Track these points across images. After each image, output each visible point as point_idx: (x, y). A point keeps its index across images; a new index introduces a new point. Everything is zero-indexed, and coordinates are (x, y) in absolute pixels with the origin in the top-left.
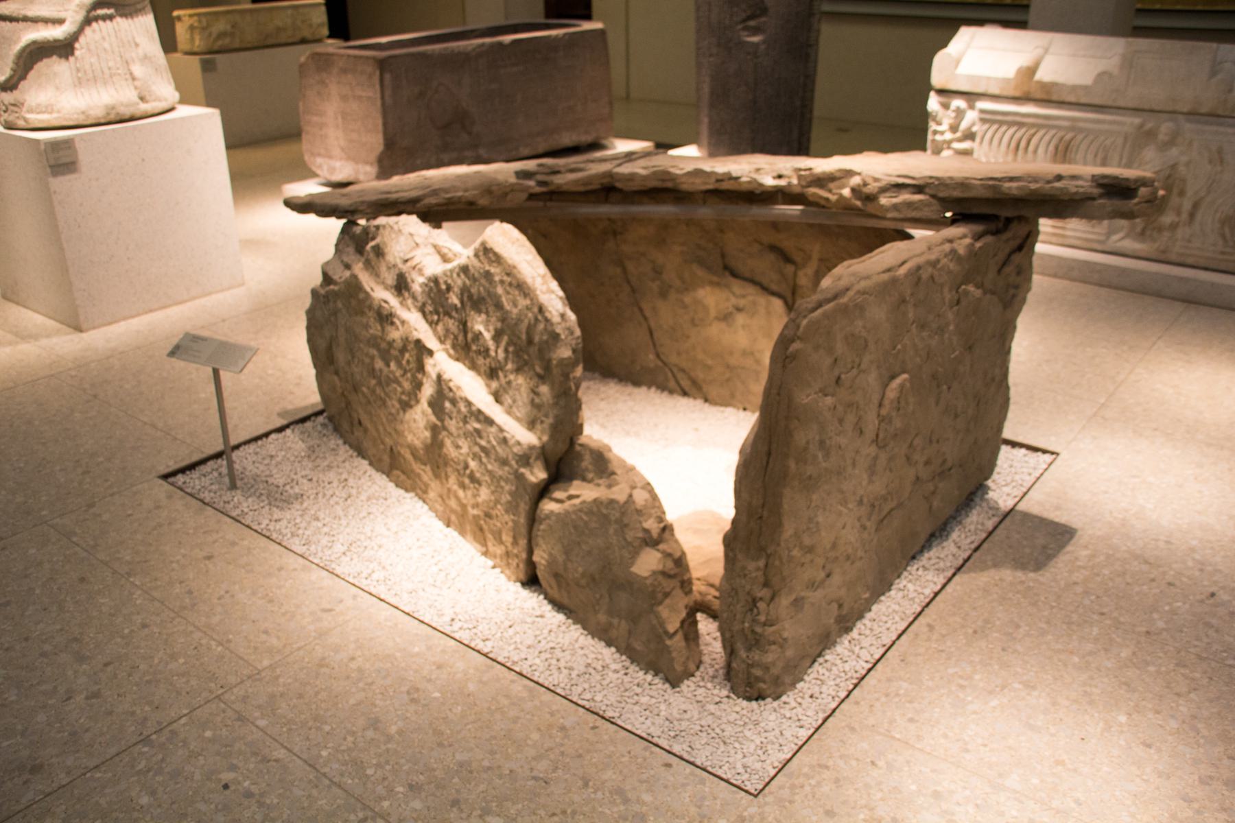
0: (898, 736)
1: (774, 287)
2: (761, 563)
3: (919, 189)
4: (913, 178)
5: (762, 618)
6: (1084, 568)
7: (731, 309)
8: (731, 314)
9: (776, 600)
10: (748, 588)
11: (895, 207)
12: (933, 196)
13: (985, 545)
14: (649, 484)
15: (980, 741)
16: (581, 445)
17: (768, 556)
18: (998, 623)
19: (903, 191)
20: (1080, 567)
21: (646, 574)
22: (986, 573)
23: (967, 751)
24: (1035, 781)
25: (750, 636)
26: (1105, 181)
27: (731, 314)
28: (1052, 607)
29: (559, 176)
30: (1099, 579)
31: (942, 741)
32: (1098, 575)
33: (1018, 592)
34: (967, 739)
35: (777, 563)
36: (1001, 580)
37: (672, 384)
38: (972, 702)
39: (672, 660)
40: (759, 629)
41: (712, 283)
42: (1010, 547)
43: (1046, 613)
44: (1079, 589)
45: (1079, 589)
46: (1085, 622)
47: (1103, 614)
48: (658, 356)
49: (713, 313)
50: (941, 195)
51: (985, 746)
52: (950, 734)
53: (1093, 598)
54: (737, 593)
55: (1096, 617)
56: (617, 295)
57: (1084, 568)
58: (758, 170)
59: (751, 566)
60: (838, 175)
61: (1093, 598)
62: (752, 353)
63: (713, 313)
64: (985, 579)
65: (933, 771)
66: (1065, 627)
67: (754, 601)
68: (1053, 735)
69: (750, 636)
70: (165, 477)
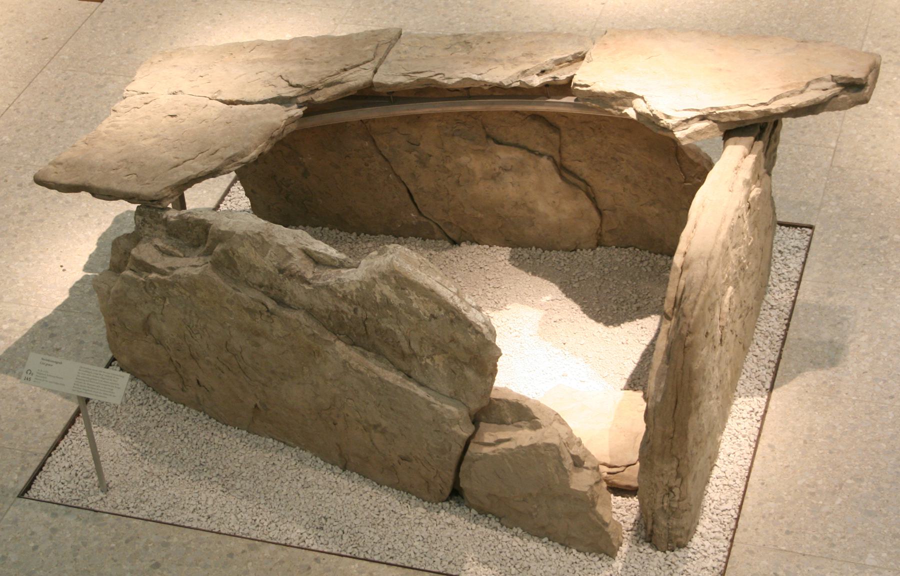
0: (784, 548)
1: (541, 149)
2: (675, 465)
3: (703, 118)
4: (698, 110)
5: (677, 498)
6: (867, 354)
7: (497, 171)
8: (499, 174)
9: (685, 483)
10: (666, 482)
11: (688, 137)
12: (715, 121)
13: (785, 353)
14: (557, 414)
15: (839, 535)
16: (497, 400)
17: (679, 460)
18: (819, 429)
19: (690, 122)
20: (864, 354)
21: (586, 489)
22: (794, 382)
23: (833, 545)
24: (884, 555)
25: (668, 510)
26: (843, 81)
27: (499, 174)
28: (854, 401)
29: (317, 93)
30: (880, 363)
31: (815, 543)
32: (878, 359)
33: (824, 395)
34: (830, 536)
35: (686, 462)
36: (808, 385)
37: (438, 234)
38: (823, 505)
39: (611, 540)
40: (675, 505)
41: (476, 152)
42: (805, 348)
43: (850, 409)
44: (869, 378)
45: (869, 378)
46: (882, 408)
47: (892, 397)
48: (420, 212)
49: (479, 175)
50: (723, 120)
51: (844, 538)
52: (818, 536)
53: (881, 383)
54: (656, 485)
55: (888, 401)
56: (366, 165)
57: (867, 354)
58: (524, 73)
59: (666, 468)
60: (618, 95)
61: (881, 383)
62: (525, 204)
63: (479, 175)
64: (795, 388)
65: (817, 568)
66: (868, 417)
67: (671, 489)
68: (885, 515)
69: (668, 510)
70: (23, 493)
